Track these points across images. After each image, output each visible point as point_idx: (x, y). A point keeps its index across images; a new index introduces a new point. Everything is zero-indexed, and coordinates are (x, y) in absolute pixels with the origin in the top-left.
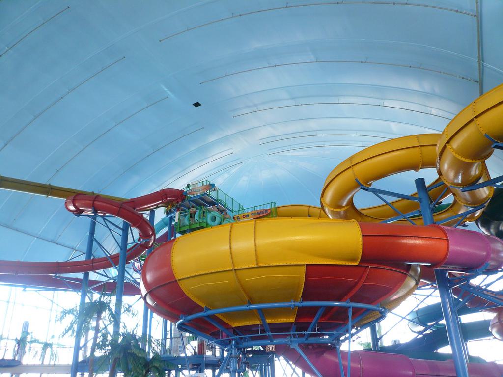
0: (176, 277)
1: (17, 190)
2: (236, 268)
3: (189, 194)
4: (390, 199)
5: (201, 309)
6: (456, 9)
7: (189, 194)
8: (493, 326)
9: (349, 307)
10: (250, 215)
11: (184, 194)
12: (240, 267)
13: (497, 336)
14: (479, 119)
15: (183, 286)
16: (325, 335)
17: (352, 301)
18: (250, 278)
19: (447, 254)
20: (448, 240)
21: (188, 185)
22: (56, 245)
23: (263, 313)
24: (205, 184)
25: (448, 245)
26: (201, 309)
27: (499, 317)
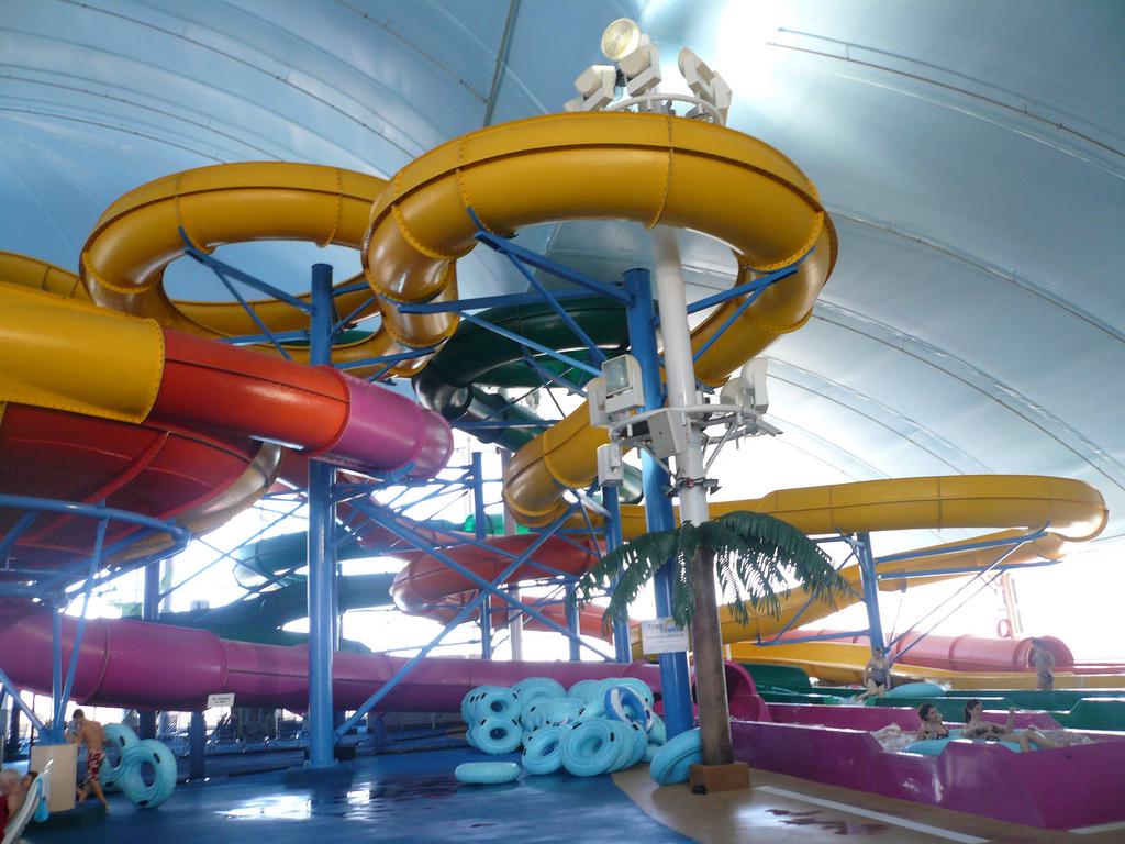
9: (103, 518)
17: (111, 504)
20: (348, 404)
25: (347, 414)
27: (411, 569)
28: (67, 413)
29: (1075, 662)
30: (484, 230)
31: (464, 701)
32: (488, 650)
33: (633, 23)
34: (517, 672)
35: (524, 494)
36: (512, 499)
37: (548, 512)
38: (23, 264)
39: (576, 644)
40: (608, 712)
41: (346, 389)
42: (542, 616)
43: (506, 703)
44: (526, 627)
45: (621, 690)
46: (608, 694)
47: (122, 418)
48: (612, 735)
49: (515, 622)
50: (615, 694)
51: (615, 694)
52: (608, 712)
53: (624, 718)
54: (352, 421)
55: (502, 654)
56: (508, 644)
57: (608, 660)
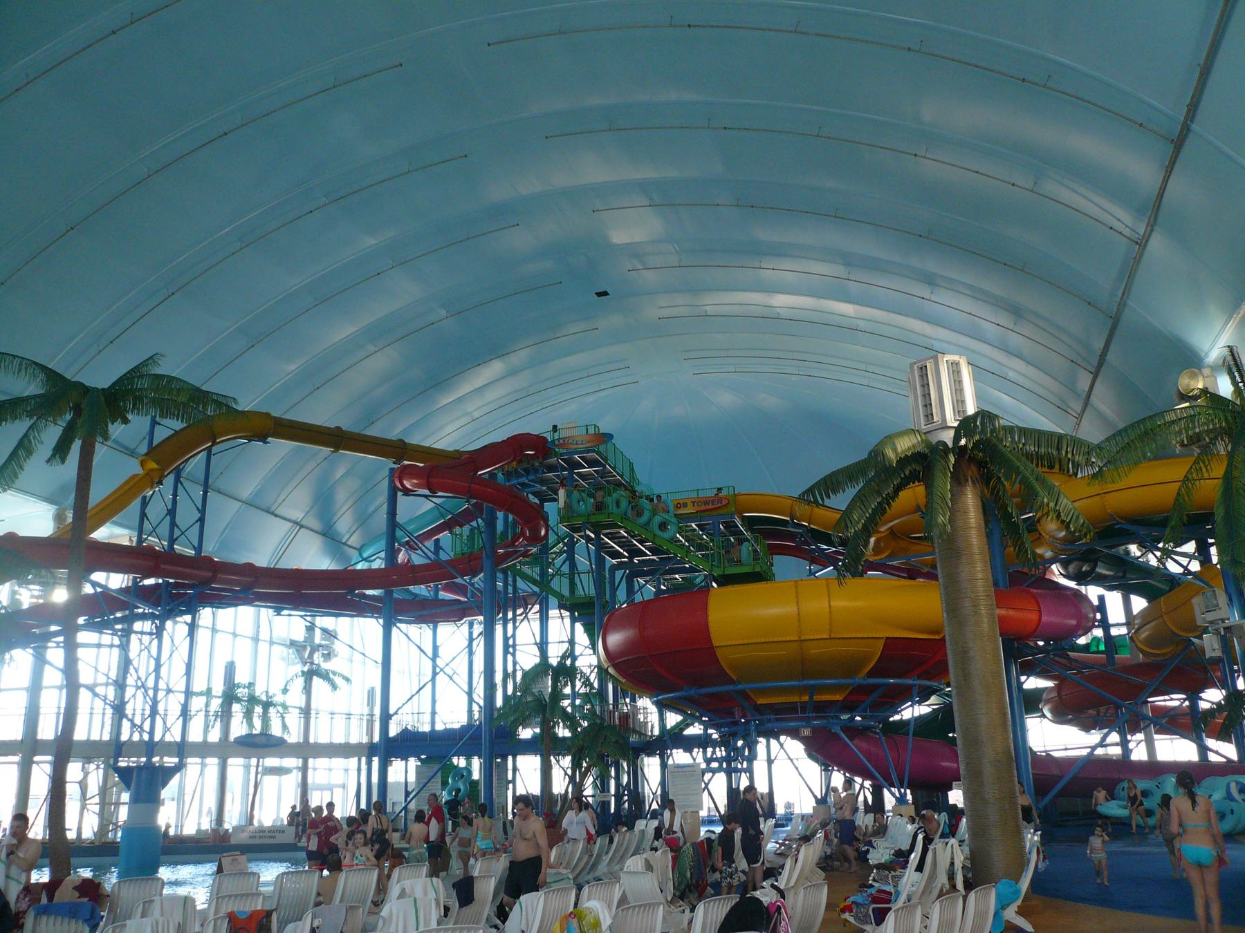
0: (713, 641)
1: (304, 443)
2: (803, 638)
3: (560, 446)
4: (949, 528)
5: (732, 682)
6: (1090, 301)
7: (560, 446)
8: (1047, 702)
9: (915, 685)
10: (690, 505)
11: (549, 445)
12: (807, 637)
13: (1048, 715)
14: (1106, 495)
15: (719, 653)
16: (140, 608)
17: (920, 677)
18: (814, 651)
19: (1037, 627)
20: (1040, 611)
21: (555, 428)
22: (273, 517)
23: (813, 690)
24: (592, 431)
25: (1040, 616)
26: (732, 682)
27: (1058, 688)
28: (907, 638)
29: (563, 792)
30: (1121, 523)
31: (1116, 791)
32: (1127, 752)
33: (1196, 370)
34: (1154, 769)
35: (1147, 638)
36: (1140, 641)
37: (1169, 650)
38: (771, 498)
39: (1203, 750)
40: (1229, 797)
41: (1037, 602)
42: (1172, 723)
43: (1152, 793)
44: (1157, 732)
45: (1237, 783)
46: (1228, 785)
47: (931, 637)
48: (605, 294)
49: (1148, 729)
50: (1233, 785)
51: (1233, 785)
52: (1229, 797)
53: (1241, 801)
54: (1045, 619)
55: (1139, 754)
56: (1143, 745)
57: (1229, 761)
